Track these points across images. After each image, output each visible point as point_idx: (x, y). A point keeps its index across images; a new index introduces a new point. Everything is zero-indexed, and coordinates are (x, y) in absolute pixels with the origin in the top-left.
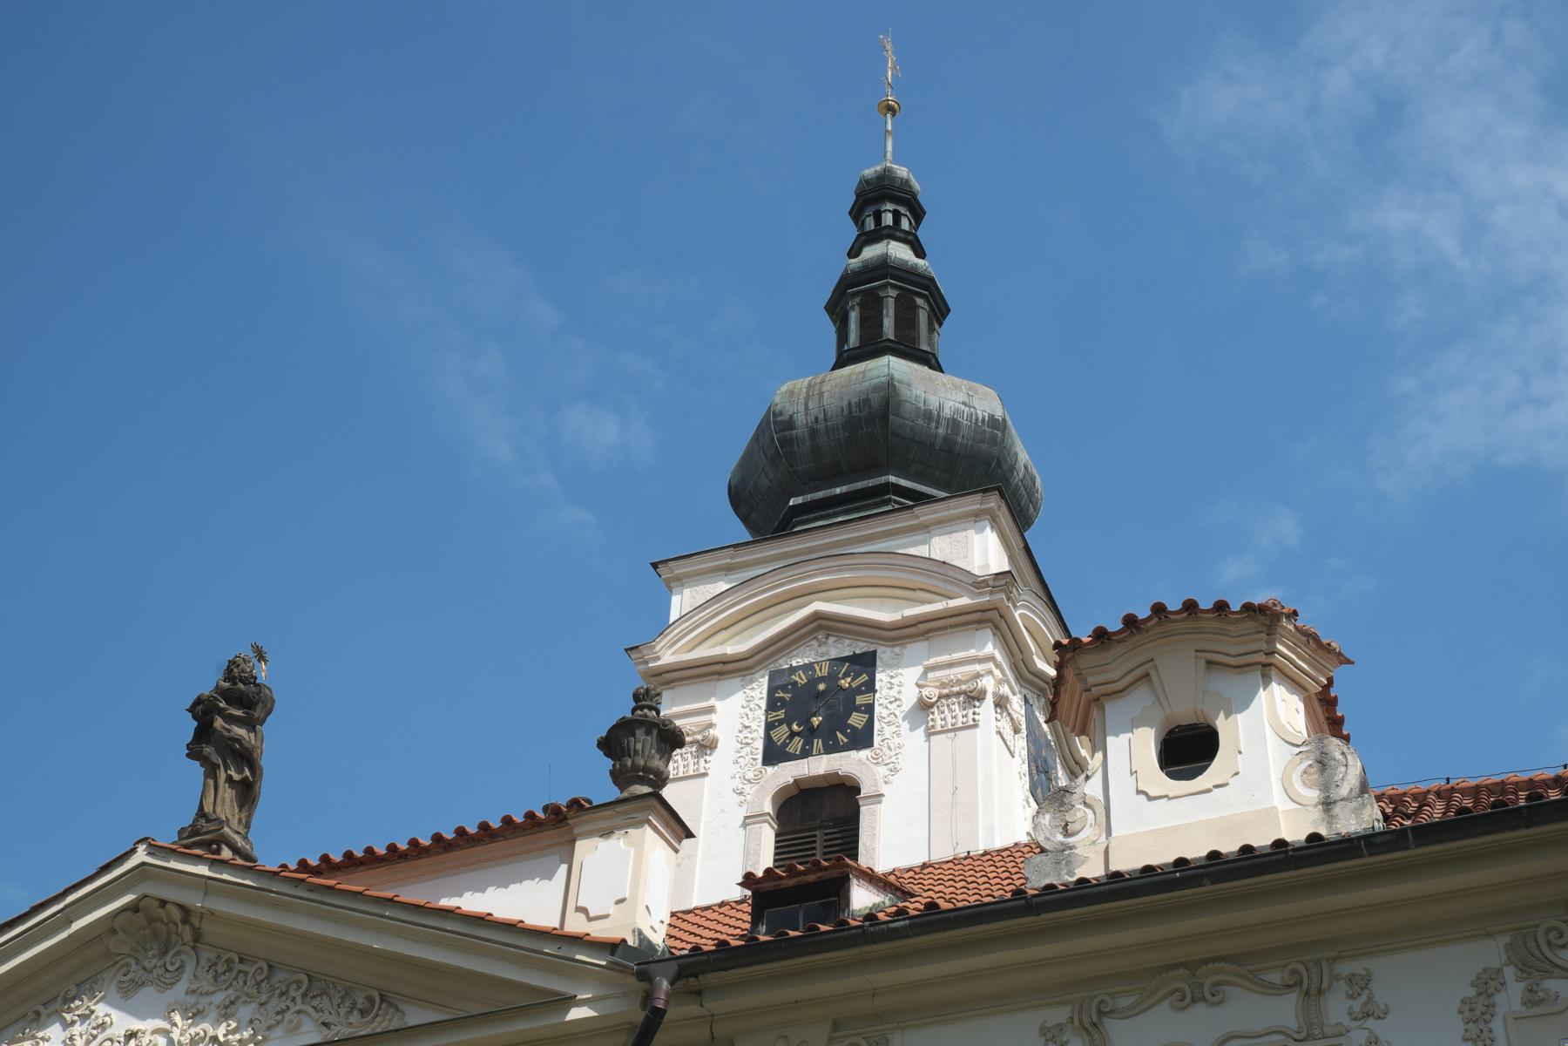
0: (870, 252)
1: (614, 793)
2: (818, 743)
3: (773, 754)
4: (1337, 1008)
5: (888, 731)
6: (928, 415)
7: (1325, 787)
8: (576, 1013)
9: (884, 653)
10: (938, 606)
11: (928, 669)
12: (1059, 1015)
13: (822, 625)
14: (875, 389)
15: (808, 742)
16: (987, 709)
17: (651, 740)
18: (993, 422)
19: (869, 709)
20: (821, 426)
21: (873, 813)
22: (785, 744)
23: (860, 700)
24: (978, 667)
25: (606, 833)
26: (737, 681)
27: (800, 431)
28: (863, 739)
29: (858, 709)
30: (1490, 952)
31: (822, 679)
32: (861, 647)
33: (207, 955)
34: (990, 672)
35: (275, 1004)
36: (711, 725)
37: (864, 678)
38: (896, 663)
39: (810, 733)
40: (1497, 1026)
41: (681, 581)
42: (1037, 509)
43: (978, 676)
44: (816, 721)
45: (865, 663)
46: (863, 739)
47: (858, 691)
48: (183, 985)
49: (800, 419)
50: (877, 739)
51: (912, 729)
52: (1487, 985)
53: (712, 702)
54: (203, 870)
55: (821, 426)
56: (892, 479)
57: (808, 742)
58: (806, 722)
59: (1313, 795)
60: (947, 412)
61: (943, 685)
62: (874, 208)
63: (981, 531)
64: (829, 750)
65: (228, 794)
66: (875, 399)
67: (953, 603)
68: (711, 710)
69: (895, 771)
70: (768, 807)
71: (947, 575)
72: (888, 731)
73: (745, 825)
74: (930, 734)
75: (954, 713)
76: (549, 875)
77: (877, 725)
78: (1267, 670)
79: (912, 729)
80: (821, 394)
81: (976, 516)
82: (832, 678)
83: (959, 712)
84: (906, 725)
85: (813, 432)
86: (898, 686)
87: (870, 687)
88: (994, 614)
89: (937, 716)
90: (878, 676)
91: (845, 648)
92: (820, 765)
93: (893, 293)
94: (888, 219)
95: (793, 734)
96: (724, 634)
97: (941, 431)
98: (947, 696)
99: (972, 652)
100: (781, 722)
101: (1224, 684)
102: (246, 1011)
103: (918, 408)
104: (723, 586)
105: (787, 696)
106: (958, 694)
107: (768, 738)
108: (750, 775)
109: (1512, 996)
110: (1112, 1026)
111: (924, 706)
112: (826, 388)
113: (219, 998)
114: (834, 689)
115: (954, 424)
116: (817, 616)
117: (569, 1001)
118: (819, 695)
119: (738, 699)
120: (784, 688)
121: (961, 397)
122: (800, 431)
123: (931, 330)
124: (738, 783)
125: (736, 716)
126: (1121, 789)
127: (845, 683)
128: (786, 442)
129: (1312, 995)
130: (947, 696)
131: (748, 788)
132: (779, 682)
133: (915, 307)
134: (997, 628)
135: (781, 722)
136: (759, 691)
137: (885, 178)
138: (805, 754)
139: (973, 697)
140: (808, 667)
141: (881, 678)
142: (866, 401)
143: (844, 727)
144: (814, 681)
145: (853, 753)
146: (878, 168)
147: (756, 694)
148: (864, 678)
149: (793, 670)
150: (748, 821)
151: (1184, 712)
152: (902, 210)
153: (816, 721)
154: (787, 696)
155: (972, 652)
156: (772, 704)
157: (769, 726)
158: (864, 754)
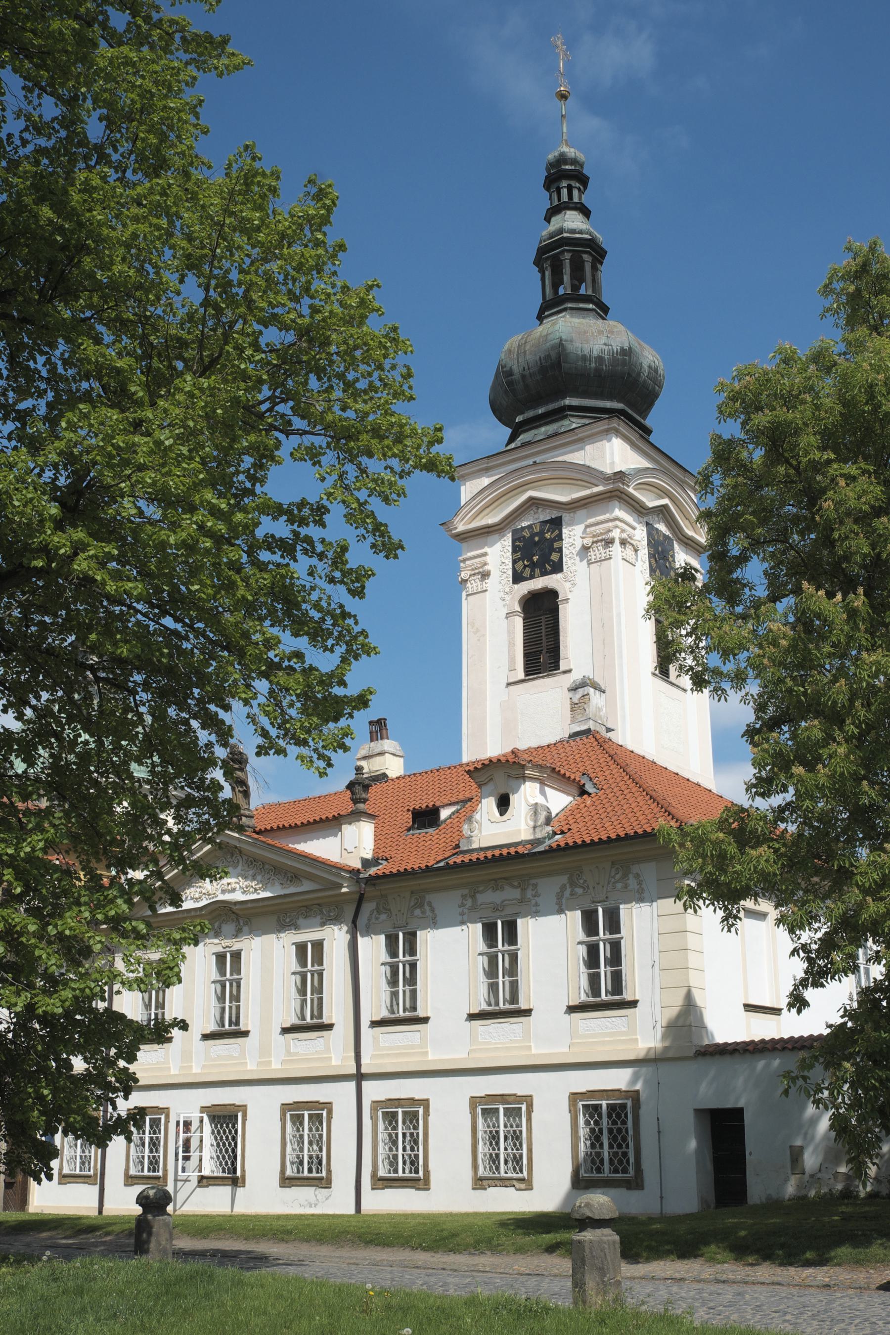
0: (556, 222)
1: (351, 807)
2: (537, 571)
3: (517, 578)
4: (529, 893)
5: (570, 562)
6: (584, 358)
7: (535, 821)
8: (344, 890)
9: (566, 517)
10: (587, 492)
11: (587, 527)
12: (466, 891)
13: (533, 503)
14: (553, 347)
15: (533, 571)
16: (616, 547)
17: (360, 788)
18: (623, 352)
19: (560, 550)
20: (527, 373)
21: (565, 609)
22: (522, 572)
23: (556, 545)
24: (610, 524)
25: (350, 824)
26: (496, 536)
27: (516, 377)
28: (558, 567)
29: (554, 550)
30: (564, 879)
31: (537, 534)
32: (555, 514)
33: (245, 858)
34: (617, 527)
35: (267, 876)
36: (486, 564)
37: (557, 532)
38: (572, 523)
39: (533, 566)
40: (564, 901)
41: (465, 478)
42: (661, 387)
43: (610, 531)
44: (535, 558)
45: (556, 523)
46: (558, 567)
47: (554, 540)
48: (240, 867)
49: (516, 370)
50: (565, 567)
51: (581, 561)
52: (563, 888)
53: (486, 549)
54: (236, 835)
55: (527, 373)
56: (568, 401)
57: (533, 571)
58: (530, 559)
59: (532, 824)
60: (595, 353)
61: (594, 536)
62: (555, 185)
63: (609, 440)
64: (544, 573)
65: (240, 796)
66: (553, 354)
67: (596, 490)
68: (485, 554)
69: (574, 585)
70: (518, 608)
71: (588, 474)
72: (570, 562)
73: (507, 618)
74: (590, 563)
75: (598, 552)
76: (336, 836)
77: (564, 559)
78: (524, 778)
79: (581, 561)
80: (525, 352)
81: (607, 432)
82: (541, 533)
83: (602, 551)
84: (578, 558)
85: (523, 377)
86: (573, 536)
87: (560, 538)
88: (618, 493)
89: (592, 553)
90: (564, 531)
91: (545, 515)
92: (538, 583)
93: (567, 256)
94: (565, 197)
95: (525, 566)
96: (488, 510)
97: (593, 365)
98: (596, 542)
99: (607, 516)
100: (519, 559)
101: (513, 783)
102: (259, 877)
103: (577, 355)
104: (486, 481)
105: (521, 544)
106: (601, 541)
107: (514, 569)
108: (507, 590)
109: (567, 893)
110: (478, 896)
111: (585, 549)
112: (527, 348)
113: (251, 873)
114: (543, 540)
115: (600, 359)
116: (531, 499)
117: (341, 886)
118: (536, 543)
119: (498, 546)
120: (519, 539)
121: (604, 340)
122: (516, 377)
123: (594, 269)
124: (502, 595)
125: (499, 555)
126: (485, 822)
127: (548, 536)
128: (510, 384)
129: (524, 890)
130: (596, 542)
131: (507, 597)
132: (517, 536)
133: (583, 261)
134: (620, 498)
135: (519, 559)
136: (506, 542)
137: (562, 159)
138: (532, 577)
139: (609, 542)
140: (530, 527)
141: (565, 531)
142: (548, 356)
143: (549, 561)
144: (533, 535)
145: (554, 576)
146: (556, 154)
147: (506, 543)
148: (557, 532)
149: (523, 528)
150: (509, 615)
151: (503, 791)
152: (573, 183)
153: (535, 558)
154: (521, 544)
155: (607, 516)
156: (515, 549)
157: (514, 562)
158: (559, 576)
